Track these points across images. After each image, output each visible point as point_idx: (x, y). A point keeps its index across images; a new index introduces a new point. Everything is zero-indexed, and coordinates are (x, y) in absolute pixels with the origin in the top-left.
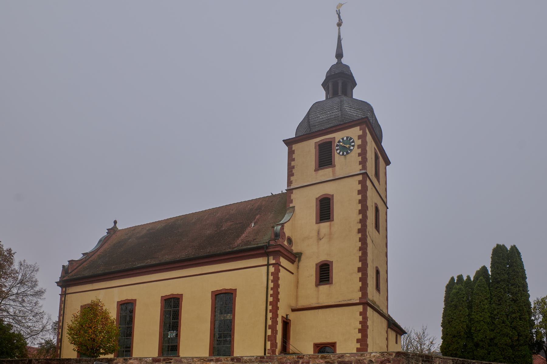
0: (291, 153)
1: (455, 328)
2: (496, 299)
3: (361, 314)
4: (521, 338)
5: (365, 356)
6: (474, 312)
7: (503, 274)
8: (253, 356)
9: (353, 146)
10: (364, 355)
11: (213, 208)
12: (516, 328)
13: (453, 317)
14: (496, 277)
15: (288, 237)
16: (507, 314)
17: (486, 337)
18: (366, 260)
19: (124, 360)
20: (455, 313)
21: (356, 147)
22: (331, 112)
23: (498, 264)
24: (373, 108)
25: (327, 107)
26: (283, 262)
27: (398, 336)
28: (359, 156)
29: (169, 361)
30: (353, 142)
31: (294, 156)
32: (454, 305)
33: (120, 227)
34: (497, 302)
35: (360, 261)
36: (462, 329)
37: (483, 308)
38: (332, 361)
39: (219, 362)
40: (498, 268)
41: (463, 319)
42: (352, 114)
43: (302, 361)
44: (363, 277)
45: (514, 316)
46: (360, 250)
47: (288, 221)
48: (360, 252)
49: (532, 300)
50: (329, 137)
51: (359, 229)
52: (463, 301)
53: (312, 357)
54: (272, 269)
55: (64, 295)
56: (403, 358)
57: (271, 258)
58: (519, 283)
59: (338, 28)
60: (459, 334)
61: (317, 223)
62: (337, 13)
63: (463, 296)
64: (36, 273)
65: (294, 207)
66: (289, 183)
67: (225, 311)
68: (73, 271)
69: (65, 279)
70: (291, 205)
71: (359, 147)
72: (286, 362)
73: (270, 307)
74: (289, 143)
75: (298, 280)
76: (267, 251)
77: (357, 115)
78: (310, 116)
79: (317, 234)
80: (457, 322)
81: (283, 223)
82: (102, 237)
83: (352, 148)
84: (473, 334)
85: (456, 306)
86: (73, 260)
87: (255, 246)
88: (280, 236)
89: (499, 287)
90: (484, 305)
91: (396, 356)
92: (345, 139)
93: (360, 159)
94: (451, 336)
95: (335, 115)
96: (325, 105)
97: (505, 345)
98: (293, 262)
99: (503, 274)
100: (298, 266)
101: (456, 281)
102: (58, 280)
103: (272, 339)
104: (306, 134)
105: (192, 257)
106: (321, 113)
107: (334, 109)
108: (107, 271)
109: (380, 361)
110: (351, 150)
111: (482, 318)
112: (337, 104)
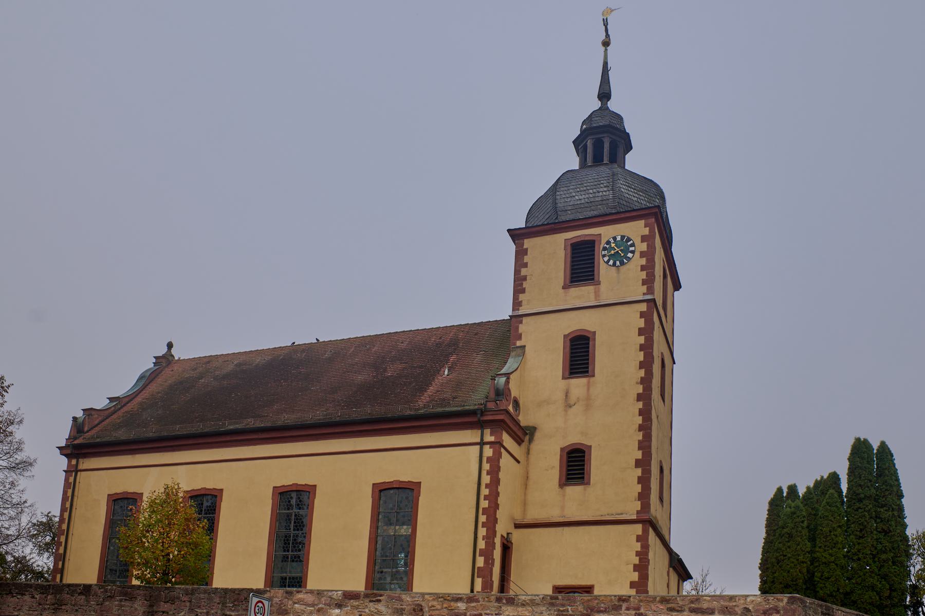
0: (521, 253)
1: (789, 572)
2: (856, 527)
3: (639, 538)
4: (894, 594)
5: (737, 601)
6: (820, 547)
7: (868, 487)
8: (538, 596)
9: (633, 252)
10: (735, 599)
11: (363, 337)
12: (887, 578)
13: (784, 554)
14: (857, 492)
15: (514, 397)
16: (874, 553)
17: (838, 589)
18: (650, 447)
19: (287, 593)
20: (789, 547)
21: (637, 254)
22: (595, 190)
23: (860, 471)
24: (664, 191)
25: (589, 181)
26: (507, 440)
27: (681, 581)
28: (527, 263)
29: (377, 598)
30: (633, 245)
31: (526, 259)
32: (788, 534)
33: (177, 353)
34: (858, 533)
35: (639, 448)
36: (800, 574)
37: (835, 542)
38: (679, 607)
39: (473, 602)
40: (860, 478)
41: (802, 557)
42: (630, 198)
43: (627, 606)
44: (644, 476)
45: (884, 556)
46: (640, 430)
47: (515, 370)
48: (639, 433)
49: (910, 532)
50: (587, 234)
51: (639, 395)
52: (803, 528)
53: (645, 599)
54: (488, 452)
55: (72, 472)
56: (799, 606)
57: (487, 431)
58: (893, 504)
59: (603, 49)
60: (794, 583)
61: (564, 378)
62: (604, 25)
63: (802, 519)
64: (17, 426)
65: (525, 346)
66: (517, 304)
67: (397, 520)
68: (92, 428)
69: (76, 442)
70: (519, 343)
71: (642, 254)
72: (596, 606)
73: (483, 518)
74: (516, 235)
75: (528, 473)
76: (481, 419)
77: (639, 200)
78: (558, 193)
79: (565, 397)
80: (793, 562)
81: (508, 374)
82: (147, 371)
83: (630, 255)
84: (817, 584)
85: (790, 536)
86: (94, 408)
87: (460, 409)
88: (503, 395)
89: (861, 509)
90: (836, 536)
91: (788, 603)
92: (619, 238)
93: (643, 275)
94: (781, 586)
95: (602, 196)
96: (584, 177)
97: (870, 604)
98: (519, 441)
99: (868, 487)
100: (529, 450)
101: (785, 494)
102: (63, 443)
103: (484, 574)
104: (548, 224)
105: (338, 419)
106: (578, 189)
107: (602, 185)
108: (166, 434)
109: (763, 610)
110: (629, 259)
111: (833, 557)
112: (606, 178)
